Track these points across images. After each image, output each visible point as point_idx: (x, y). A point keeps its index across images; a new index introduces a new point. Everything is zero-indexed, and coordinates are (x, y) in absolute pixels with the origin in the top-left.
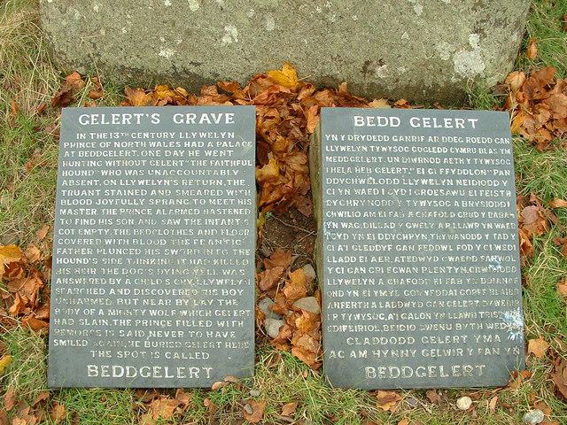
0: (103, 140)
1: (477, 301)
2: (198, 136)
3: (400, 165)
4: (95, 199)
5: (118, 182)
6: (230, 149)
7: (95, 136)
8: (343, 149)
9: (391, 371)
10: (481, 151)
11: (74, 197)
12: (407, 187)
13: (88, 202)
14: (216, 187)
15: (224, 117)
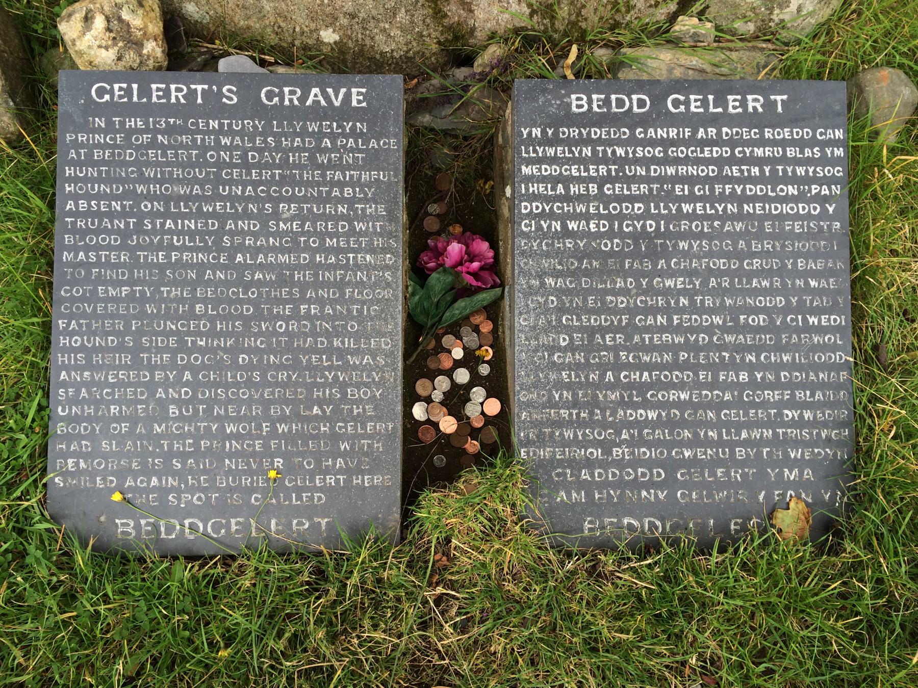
1: (773, 412)
2: (304, 128)
3: (647, 180)
4: (125, 234)
6: (360, 151)
7: (122, 123)
8: (551, 152)
9: (187, 525)
10: (791, 152)
12: (657, 218)
13: (113, 240)
14: (337, 218)
15: (348, 96)
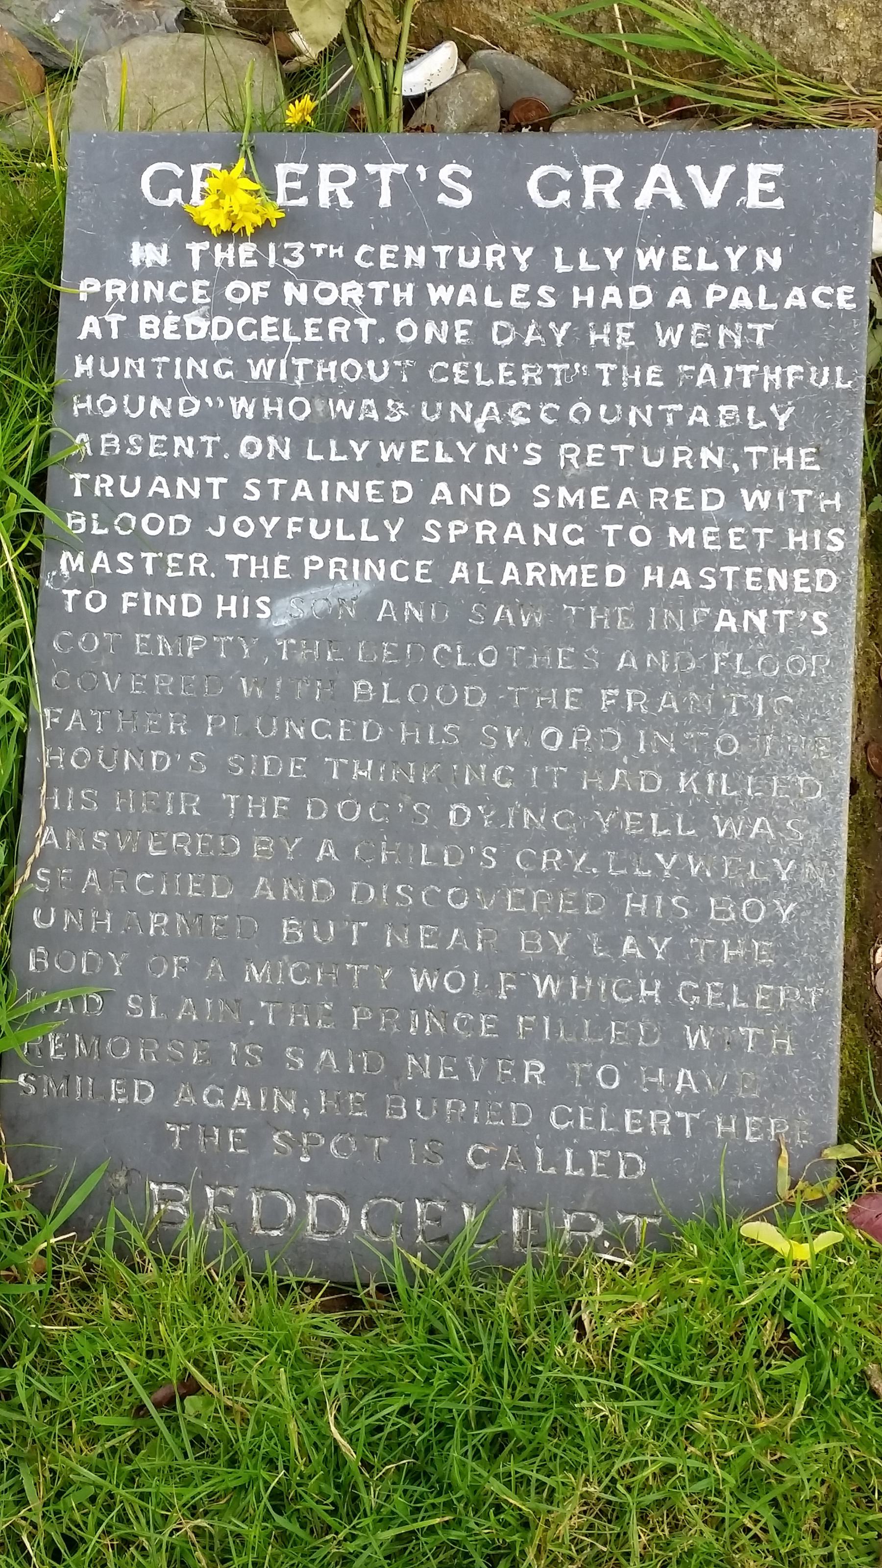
0: (238, 273)
5: (299, 450)
11: (117, 504)
